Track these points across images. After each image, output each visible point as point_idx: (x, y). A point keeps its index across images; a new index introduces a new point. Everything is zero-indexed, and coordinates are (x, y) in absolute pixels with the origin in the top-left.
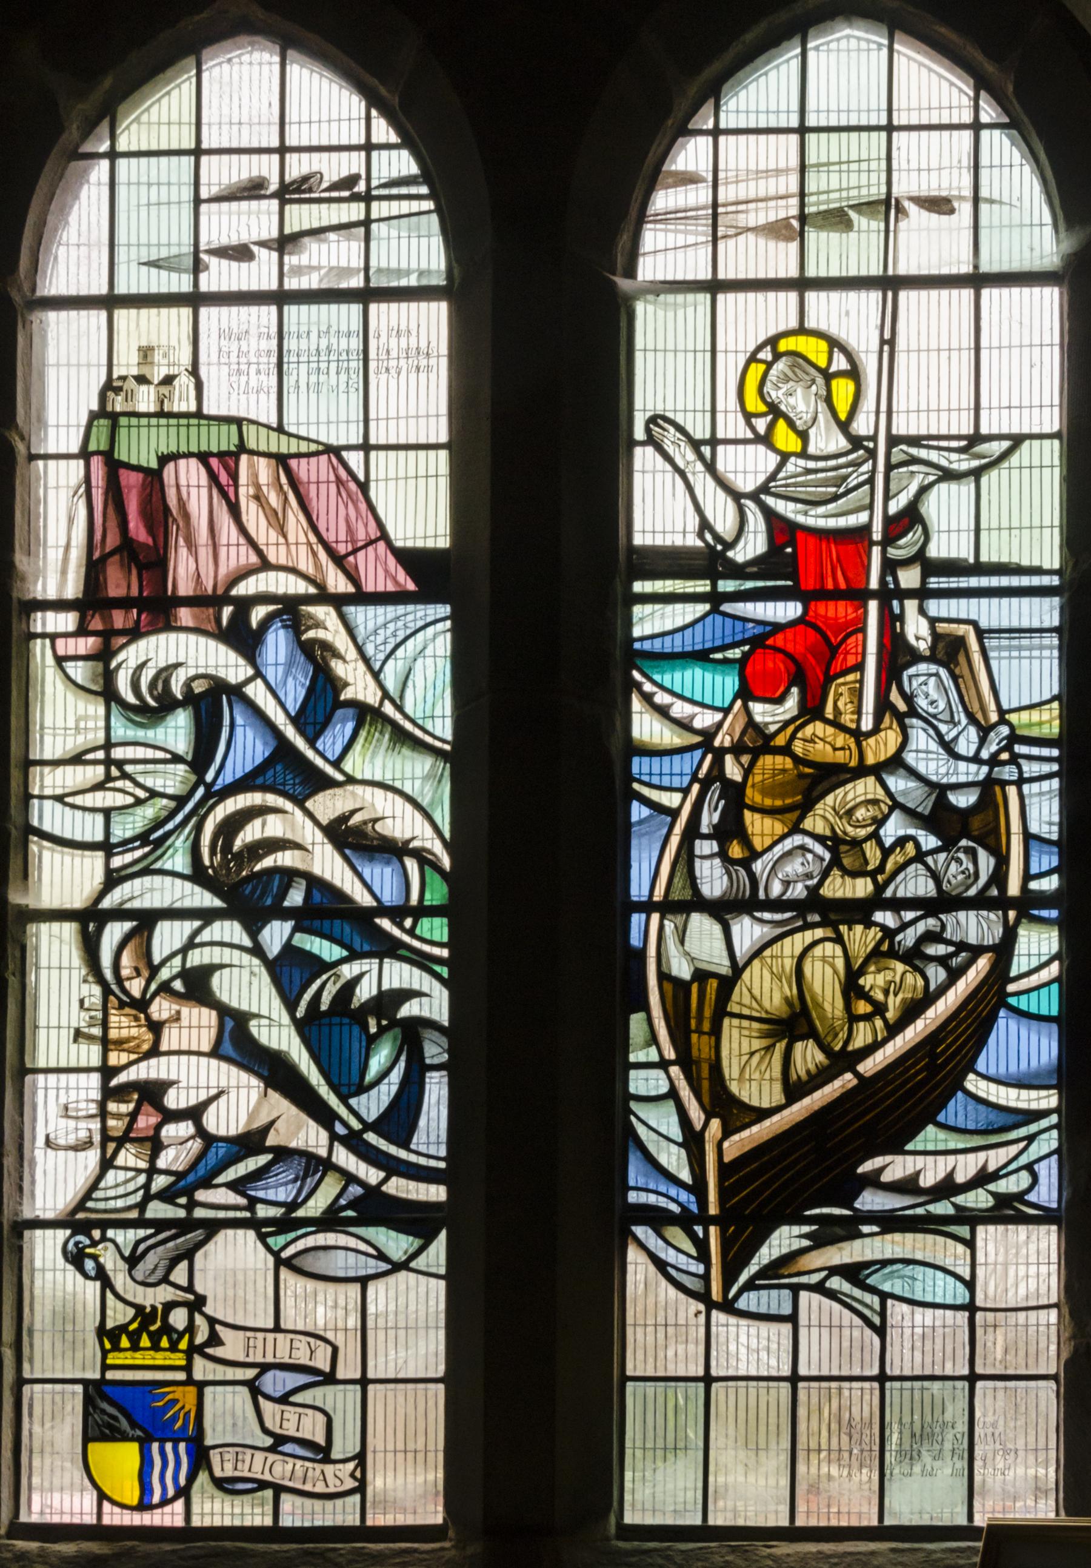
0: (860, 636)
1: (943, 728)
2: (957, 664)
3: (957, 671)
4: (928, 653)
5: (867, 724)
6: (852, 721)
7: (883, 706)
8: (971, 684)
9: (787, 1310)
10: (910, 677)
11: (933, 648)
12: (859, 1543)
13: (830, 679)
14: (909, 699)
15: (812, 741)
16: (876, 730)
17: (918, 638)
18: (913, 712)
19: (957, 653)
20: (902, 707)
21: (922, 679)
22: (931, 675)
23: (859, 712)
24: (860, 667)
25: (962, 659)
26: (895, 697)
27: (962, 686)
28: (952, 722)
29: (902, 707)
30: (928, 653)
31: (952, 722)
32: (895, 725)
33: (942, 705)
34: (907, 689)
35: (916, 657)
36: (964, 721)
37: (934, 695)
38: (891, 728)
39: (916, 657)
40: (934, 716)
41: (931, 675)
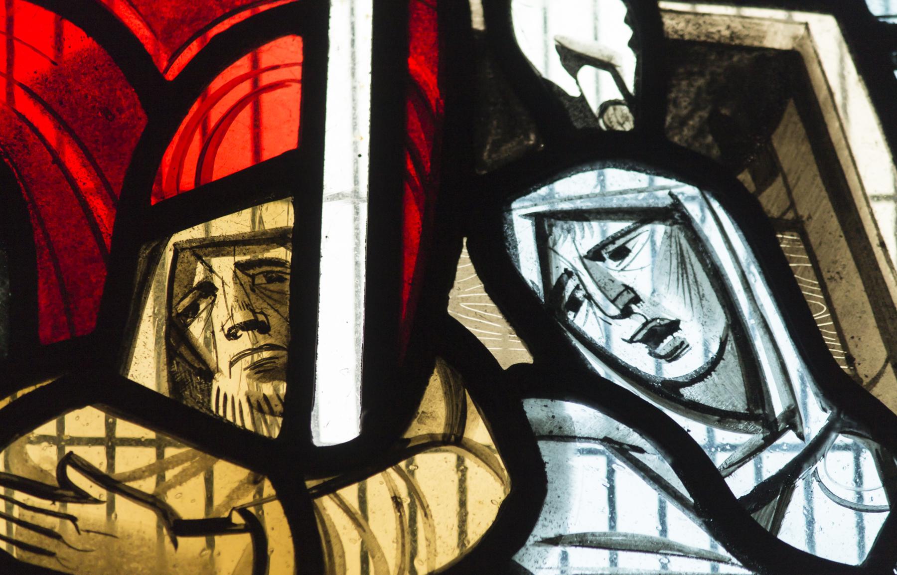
0: (287, 50)
1: (721, 443)
2: (771, 170)
3: (772, 201)
4: (622, 120)
5: (337, 418)
6: (259, 406)
7: (408, 341)
8: (841, 255)
9: (617, 302)
10: (543, 224)
11: (646, 98)
12: (842, 162)
13: (152, 212)
14: (540, 314)
15: (63, 491)
16: (384, 441)
17: (573, 60)
18: (561, 366)
19: (770, 121)
20: (507, 348)
21: (591, 235)
22: (645, 216)
23: (295, 364)
24: (298, 175)
25: (790, 147)
26: (470, 302)
27: (799, 264)
28: (758, 414)
29: (507, 348)
30: (622, 120)
31: (758, 414)
32: (478, 432)
33: (701, 335)
34: (529, 270)
35: (568, 138)
36: (816, 417)
37: (671, 303)
38: (453, 438)
39: (568, 138)
40: (670, 391)
41: (645, 216)
